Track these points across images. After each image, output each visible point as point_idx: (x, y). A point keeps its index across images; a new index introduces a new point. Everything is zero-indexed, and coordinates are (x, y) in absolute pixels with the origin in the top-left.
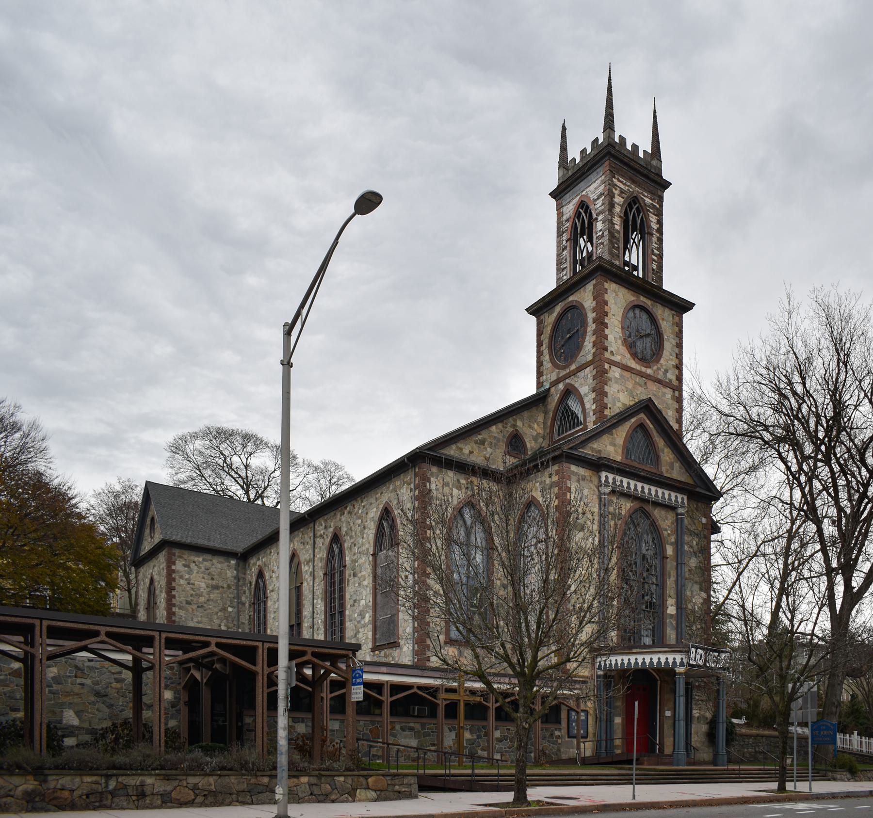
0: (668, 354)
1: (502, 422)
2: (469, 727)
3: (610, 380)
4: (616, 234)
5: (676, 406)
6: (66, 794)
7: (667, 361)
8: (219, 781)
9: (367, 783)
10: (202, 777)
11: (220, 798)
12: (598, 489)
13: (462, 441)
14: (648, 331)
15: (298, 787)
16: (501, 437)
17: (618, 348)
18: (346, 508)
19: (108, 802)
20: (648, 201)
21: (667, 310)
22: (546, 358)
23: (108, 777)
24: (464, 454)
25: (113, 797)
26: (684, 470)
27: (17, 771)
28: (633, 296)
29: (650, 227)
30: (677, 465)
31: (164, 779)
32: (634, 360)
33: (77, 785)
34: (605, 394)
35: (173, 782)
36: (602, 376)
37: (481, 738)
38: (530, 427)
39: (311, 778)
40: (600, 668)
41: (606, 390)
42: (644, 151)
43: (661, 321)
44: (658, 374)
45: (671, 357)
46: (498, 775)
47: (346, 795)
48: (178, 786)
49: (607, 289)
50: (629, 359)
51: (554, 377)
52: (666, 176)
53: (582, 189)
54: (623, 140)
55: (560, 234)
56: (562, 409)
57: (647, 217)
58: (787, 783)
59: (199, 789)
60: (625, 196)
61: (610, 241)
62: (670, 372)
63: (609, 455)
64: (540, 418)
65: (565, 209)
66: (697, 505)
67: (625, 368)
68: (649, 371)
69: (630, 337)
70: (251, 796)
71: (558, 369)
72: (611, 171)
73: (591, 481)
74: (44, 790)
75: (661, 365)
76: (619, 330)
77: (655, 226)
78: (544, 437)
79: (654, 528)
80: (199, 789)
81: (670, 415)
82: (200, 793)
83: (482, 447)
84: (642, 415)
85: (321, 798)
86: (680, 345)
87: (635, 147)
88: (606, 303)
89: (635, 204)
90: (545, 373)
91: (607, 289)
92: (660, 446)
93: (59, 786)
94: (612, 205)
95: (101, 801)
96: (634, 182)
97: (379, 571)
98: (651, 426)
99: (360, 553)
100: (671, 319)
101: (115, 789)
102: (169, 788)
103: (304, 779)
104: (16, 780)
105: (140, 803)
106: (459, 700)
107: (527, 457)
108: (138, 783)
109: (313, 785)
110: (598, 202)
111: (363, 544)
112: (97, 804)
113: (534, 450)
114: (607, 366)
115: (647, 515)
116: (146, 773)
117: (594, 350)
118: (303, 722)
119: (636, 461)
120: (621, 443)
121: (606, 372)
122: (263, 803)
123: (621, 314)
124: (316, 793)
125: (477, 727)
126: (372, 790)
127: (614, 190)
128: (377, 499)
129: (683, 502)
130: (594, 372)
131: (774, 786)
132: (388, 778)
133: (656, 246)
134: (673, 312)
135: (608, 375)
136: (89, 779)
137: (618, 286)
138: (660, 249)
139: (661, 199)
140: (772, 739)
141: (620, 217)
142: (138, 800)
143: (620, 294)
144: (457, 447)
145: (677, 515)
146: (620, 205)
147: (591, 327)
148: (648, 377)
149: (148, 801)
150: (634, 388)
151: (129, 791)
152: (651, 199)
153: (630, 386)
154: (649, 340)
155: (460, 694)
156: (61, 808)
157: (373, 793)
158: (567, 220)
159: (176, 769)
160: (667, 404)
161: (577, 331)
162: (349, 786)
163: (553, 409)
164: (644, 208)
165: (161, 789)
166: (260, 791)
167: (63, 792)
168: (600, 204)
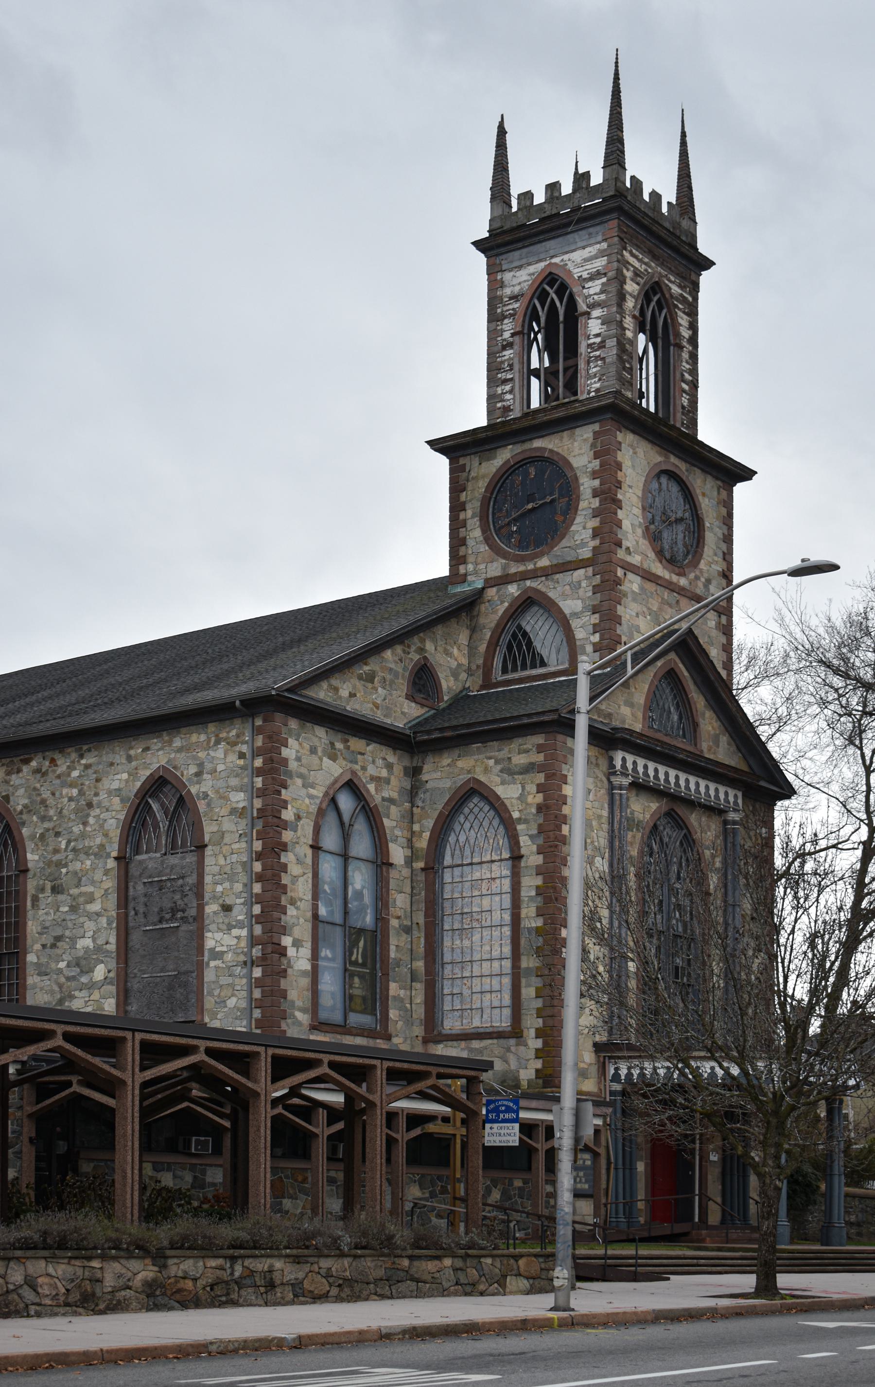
0: (711, 553)
1: (402, 643)
2: (417, 1177)
3: (625, 595)
4: (627, 346)
5: (723, 640)
6: (189, 1284)
7: (709, 564)
8: (354, 1264)
9: (518, 1267)
10: (336, 1259)
11: (357, 1287)
12: (609, 780)
13: (337, 675)
14: (680, 514)
15: (441, 1273)
16: (401, 671)
17: (637, 542)
18: (27, 761)
19: (234, 1296)
20: (675, 289)
21: (709, 479)
22: (474, 533)
23: (233, 1259)
24: (340, 697)
25: (240, 1289)
26: (734, 748)
27: (137, 1251)
28: (660, 454)
29: (678, 335)
30: (724, 739)
31: (294, 1262)
32: (661, 562)
33: (200, 1272)
34: (618, 620)
35: (305, 1266)
36: (613, 590)
37: (436, 1196)
38: (448, 653)
39: (456, 1260)
40: (616, 1077)
41: (619, 613)
42: (669, 203)
43: (700, 498)
44: (696, 586)
45: (716, 558)
46: (636, 1257)
47: (496, 1285)
48: (310, 1271)
49: (620, 443)
50: (654, 561)
51: (495, 569)
52: (704, 247)
53: (552, 252)
54: (637, 183)
55: (494, 317)
56: (512, 628)
57: (674, 318)
58: (778, 1275)
59: (332, 1276)
60: (642, 281)
61: (619, 357)
62: (714, 583)
63: (624, 722)
64: (463, 637)
65: (507, 276)
66: (754, 807)
67: (648, 576)
68: (683, 582)
69: (653, 523)
70: (390, 1286)
71: (505, 558)
72: (621, 239)
73: (597, 765)
74: (164, 1278)
75: (701, 571)
76: (637, 511)
77: (686, 333)
78: (470, 672)
79: (689, 841)
80: (332, 1276)
81: (714, 653)
82: (334, 1282)
83: (370, 685)
84: (672, 656)
85: (468, 1289)
86: (728, 539)
87: (656, 196)
88: (619, 466)
89: (655, 294)
90: (471, 559)
91: (620, 443)
92: (698, 706)
93: (180, 1274)
94: (622, 297)
95: (228, 1294)
96: (654, 257)
97: (137, 889)
98: (686, 674)
99: (74, 850)
100: (715, 493)
101: (241, 1277)
102: (301, 1275)
103: (448, 1262)
104: (135, 1265)
105: (269, 1297)
106: (454, 1135)
107: (442, 705)
108: (266, 1268)
109: (457, 1269)
110: (590, 284)
111: (83, 836)
112: (224, 1299)
113: (453, 694)
114: (620, 572)
115: (680, 824)
116: (276, 1253)
117: (593, 543)
118: (169, 1170)
119: (660, 731)
120: (642, 701)
121: (618, 582)
122: (404, 1297)
123: (641, 485)
124: (462, 1281)
125: (429, 1178)
126: (524, 1277)
127: (625, 271)
128: (130, 759)
129: (735, 803)
130: (597, 579)
131: (748, 1282)
132: (541, 1260)
133: (688, 366)
134: (719, 483)
135: (622, 588)
136: (213, 1263)
137: (637, 437)
138: (694, 372)
139: (695, 288)
140: (868, 1201)
141: (634, 317)
142: (266, 1293)
143: (640, 451)
144: (330, 685)
145: (725, 822)
146: (633, 297)
147: (588, 502)
148: (681, 591)
149: (279, 1295)
150: (660, 609)
151: (257, 1279)
152: (680, 286)
153: (655, 605)
154: (681, 528)
155: (454, 1125)
156: (185, 1305)
157: (525, 1281)
158: (514, 298)
159: (307, 1247)
160: (709, 637)
161: (553, 501)
162: (497, 1271)
163: (493, 625)
164: (670, 302)
165: (293, 1277)
166: (400, 1279)
167: (186, 1281)
168: (597, 289)
